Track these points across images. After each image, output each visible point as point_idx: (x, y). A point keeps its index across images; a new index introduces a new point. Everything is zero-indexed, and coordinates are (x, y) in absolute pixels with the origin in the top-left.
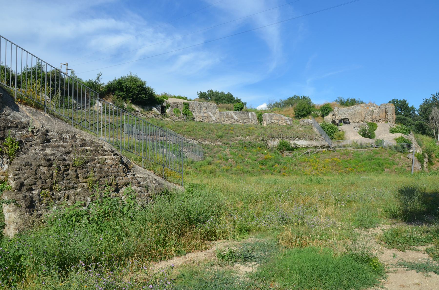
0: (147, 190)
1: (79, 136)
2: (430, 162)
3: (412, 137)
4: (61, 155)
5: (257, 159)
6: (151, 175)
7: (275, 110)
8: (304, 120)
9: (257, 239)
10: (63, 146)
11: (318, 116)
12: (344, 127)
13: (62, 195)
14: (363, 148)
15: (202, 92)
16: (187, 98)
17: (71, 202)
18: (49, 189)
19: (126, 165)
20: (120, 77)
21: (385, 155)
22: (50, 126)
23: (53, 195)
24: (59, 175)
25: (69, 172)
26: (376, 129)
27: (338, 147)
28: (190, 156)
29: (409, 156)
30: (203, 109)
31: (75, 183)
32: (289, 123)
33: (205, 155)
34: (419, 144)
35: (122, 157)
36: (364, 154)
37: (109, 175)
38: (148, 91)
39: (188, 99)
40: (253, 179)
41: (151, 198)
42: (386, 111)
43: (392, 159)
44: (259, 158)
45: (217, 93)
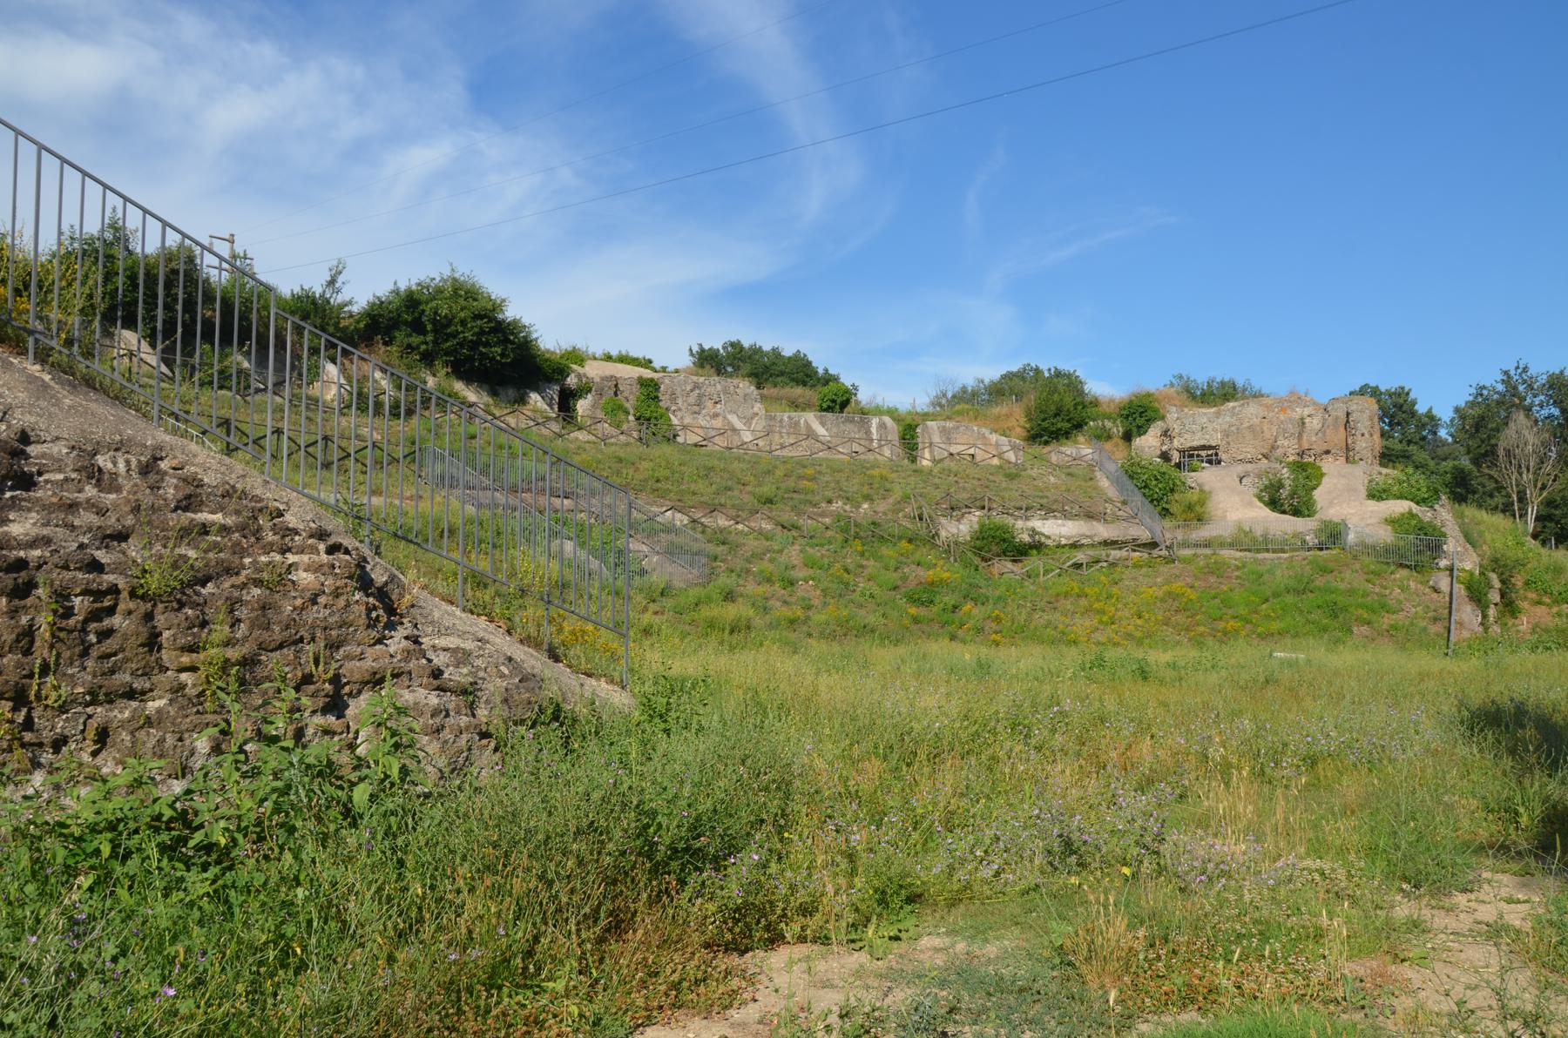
0: (472, 707)
1: (175, 463)
2: (1509, 606)
3: (1444, 515)
4: (81, 546)
5: (900, 583)
6: (492, 638)
7: (960, 413)
8: (1063, 449)
9: (961, 946)
10: (93, 505)
11: (1109, 437)
12: (1206, 477)
13: (74, 728)
14: (1274, 551)
15: (706, 347)
16: (650, 361)
17: (114, 758)
18: (7, 699)
19: (382, 594)
20: (414, 281)
21: (1350, 578)
22: (38, 415)
23: (28, 724)
24: (62, 635)
25: (116, 621)
26: (1318, 485)
27: (1185, 544)
28: (661, 570)
29: (1436, 583)
30: (709, 404)
31: (140, 672)
32: (1013, 459)
33: (714, 564)
34: (1468, 538)
35: (365, 560)
36: (1278, 573)
37: (301, 640)
38: (513, 334)
39: (657, 364)
40: (884, 656)
41: (484, 742)
42: (1348, 422)
43: (1377, 590)
44: (905, 578)
45: (756, 351)
